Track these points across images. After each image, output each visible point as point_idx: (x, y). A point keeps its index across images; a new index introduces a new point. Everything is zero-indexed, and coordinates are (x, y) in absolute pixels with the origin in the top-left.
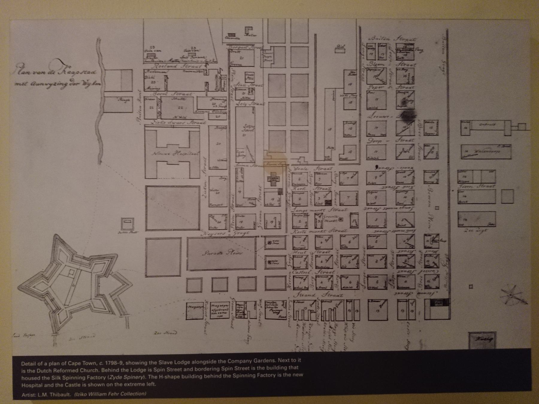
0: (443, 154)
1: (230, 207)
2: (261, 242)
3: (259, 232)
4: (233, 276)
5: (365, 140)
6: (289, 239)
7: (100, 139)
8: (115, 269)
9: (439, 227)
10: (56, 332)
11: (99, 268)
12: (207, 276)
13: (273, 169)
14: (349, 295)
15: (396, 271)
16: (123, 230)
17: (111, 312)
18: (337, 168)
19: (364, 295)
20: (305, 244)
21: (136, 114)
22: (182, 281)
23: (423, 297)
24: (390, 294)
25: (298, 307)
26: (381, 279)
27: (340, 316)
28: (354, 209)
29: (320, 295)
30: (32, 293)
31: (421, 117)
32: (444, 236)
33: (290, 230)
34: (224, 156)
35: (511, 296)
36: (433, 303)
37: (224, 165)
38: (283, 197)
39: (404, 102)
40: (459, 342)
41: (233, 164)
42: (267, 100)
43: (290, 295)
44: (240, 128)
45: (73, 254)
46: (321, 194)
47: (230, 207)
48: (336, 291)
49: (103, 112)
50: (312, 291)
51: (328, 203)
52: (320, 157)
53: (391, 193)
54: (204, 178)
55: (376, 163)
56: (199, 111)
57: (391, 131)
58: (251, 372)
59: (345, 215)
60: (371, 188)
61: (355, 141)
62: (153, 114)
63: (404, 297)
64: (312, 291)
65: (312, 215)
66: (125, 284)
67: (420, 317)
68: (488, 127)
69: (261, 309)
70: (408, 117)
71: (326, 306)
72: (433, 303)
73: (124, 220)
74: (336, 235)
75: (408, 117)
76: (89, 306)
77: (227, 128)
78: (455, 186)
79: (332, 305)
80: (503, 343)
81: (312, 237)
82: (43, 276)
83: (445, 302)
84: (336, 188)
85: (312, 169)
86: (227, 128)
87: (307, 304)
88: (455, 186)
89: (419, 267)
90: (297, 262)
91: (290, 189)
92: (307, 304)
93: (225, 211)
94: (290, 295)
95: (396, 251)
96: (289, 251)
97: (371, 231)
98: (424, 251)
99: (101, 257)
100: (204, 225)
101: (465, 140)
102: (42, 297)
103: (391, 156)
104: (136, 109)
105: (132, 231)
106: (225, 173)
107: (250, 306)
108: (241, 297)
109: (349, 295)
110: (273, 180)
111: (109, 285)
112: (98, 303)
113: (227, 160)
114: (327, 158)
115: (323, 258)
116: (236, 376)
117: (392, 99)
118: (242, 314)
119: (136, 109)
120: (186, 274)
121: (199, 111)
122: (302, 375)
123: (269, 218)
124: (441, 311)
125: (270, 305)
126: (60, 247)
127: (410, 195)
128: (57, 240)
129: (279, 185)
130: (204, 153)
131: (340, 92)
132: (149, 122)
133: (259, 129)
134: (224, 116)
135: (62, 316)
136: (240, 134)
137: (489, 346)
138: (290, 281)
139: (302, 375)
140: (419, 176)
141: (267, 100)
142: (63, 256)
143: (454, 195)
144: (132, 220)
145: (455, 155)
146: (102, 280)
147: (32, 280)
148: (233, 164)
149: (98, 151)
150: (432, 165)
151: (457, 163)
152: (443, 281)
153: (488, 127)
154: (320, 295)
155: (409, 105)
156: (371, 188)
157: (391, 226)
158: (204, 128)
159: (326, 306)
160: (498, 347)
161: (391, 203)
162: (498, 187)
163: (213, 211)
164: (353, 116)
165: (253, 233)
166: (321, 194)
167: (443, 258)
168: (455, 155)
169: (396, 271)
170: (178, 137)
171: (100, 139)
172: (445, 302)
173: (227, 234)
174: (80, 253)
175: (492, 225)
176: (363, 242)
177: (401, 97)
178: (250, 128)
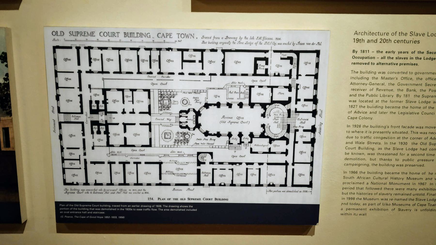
122: (123, 217)
139: (123, 217)
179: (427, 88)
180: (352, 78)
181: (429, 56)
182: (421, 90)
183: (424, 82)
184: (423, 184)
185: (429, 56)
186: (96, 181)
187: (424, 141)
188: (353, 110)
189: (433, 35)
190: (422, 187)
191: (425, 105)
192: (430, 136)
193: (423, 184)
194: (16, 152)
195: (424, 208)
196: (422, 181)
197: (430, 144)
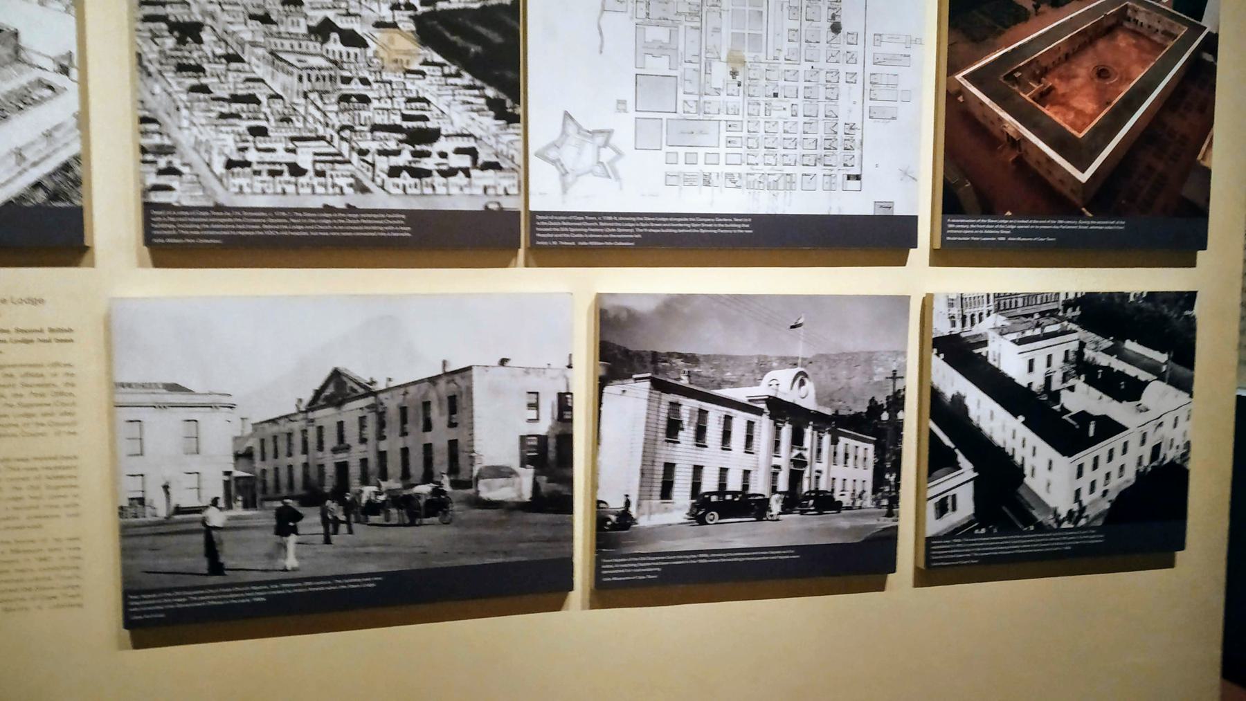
0: (860, 61)
1: (700, 95)
2: (723, 124)
3: (723, 116)
4: (701, 151)
5: (804, 44)
6: (745, 124)
7: (601, 33)
8: (613, 141)
9: (855, 119)
10: (565, 190)
11: (600, 140)
12: (682, 151)
13: (734, 65)
14: (788, 170)
15: (824, 152)
16: (619, 110)
17: (609, 177)
18: (784, 67)
19: (798, 170)
20: (756, 129)
21: (629, 14)
22: (661, 154)
23: (842, 172)
24: (819, 170)
25: (751, 178)
26: (813, 158)
27: (781, 187)
28: (794, 101)
29: (767, 169)
30: (546, 159)
31: (845, 30)
32: (858, 125)
33: (746, 116)
34: (697, 52)
35: (906, 174)
36: (849, 178)
37: (696, 59)
38: (741, 88)
39: (833, 17)
40: (869, 210)
41: (703, 59)
42: (731, 7)
43: (745, 169)
44: (710, 29)
45: (579, 128)
46: (770, 87)
47: (700, 95)
48: (780, 167)
49: (603, 10)
50: (761, 166)
51: (776, 95)
52: (771, 57)
53: (822, 89)
54: (681, 70)
55: (810, 64)
56: (678, 13)
57: (823, 39)
58: (713, 228)
59: (788, 106)
60: (808, 84)
61: (797, 45)
62: (642, 14)
63: (827, 172)
64: (761, 166)
65: (763, 104)
66: (619, 154)
67: (840, 189)
68: (52, 463)
69: (722, 179)
70: (836, 28)
71: (771, 178)
72: (849, 178)
73: (619, 102)
74: (781, 122)
75: (836, 28)
76: (591, 171)
77: (700, 29)
78: (868, 86)
79: (775, 178)
80: (898, 212)
81: (762, 122)
82: (555, 145)
83: (858, 177)
84: (782, 83)
85: (764, 66)
86: (700, 29)
87: (757, 177)
88: (868, 86)
89: (840, 149)
90: (752, 143)
91: (747, 82)
92: (757, 177)
93: (696, 98)
94: (745, 169)
95: (825, 136)
96: (745, 134)
97: (807, 119)
98: (845, 137)
99: (601, 132)
100: (680, 110)
101: (877, 50)
102: (553, 162)
103: (823, 59)
104: (630, 9)
105: (625, 111)
106: (697, 66)
107: (714, 177)
108: (708, 169)
109: (788, 170)
110: (734, 74)
111: (607, 155)
112: (598, 169)
113: (699, 55)
114: (776, 58)
115: (771, 140)
116: (703, 231)
117: (825, 14)
118: (707, 183)
119: (630, 9)
120: (666, 149)
121: (678, 13)
122: (1004, 508)
123: (730, 105)
124: (854, 184)
125: (729, 176)
126: (569, 121)
127: (835, 91)
128: (567, 115)
129: (739, 78)
130: (681, 48)
131: (786, 5)
132: (639, 21)
133: (724, 31)
134: (697, 19)
135: (569, 178)
136: (709, 33)
137: (888, 212)
138: (744, 157)
139: (1004, 508)
140: (842, 76)
141: (731, 7)
142: (571, 129)
143: (867, 92)
144: (624, 102)
145: (869, 62)
146: (603, 150)
147: (548, 148)
148: (703, 59)
149: (598, 43)
150: (852, 68)
151: (870, 68)
152: (856, 161)
153: (52, 463)
154: (767, 169)
155: (837, 19)
156: (808, 84)
157: (821, 116)
158: (681, 28)
159: (771, 178)
160: (896, 213)
161: (822, 98)
162: (900, 88)
163: (687, 97)
164: (795, 25)
165: (717, 117)
166: (770, 87)
167: (857, 142)
168: (869, 62)
169: (824, 152)
170: (661, 34)
171: (601, 33)
172: (858, 177)
173: (697, 117)
174: (586, 128)
175: (894, 118)
176: (800, 129)
177: (831, 12)
178: (717, 30)
179: (25, 391)
180: (74, 404)
181: (20, 336)
182: (16, 395)
183: (18, 381)
184: (45, 559)
185: (20, 336)
186: (444, 364)
187: (35, 483)
188: (69, 501)
189: (4, 301)
190: (44, 565)
191: (25, 420)
192: (44, 473)
193: (45, 559)
194: (1218, 670)
195: (55, 602)
196: (42, 555)
197: (48, 487)
